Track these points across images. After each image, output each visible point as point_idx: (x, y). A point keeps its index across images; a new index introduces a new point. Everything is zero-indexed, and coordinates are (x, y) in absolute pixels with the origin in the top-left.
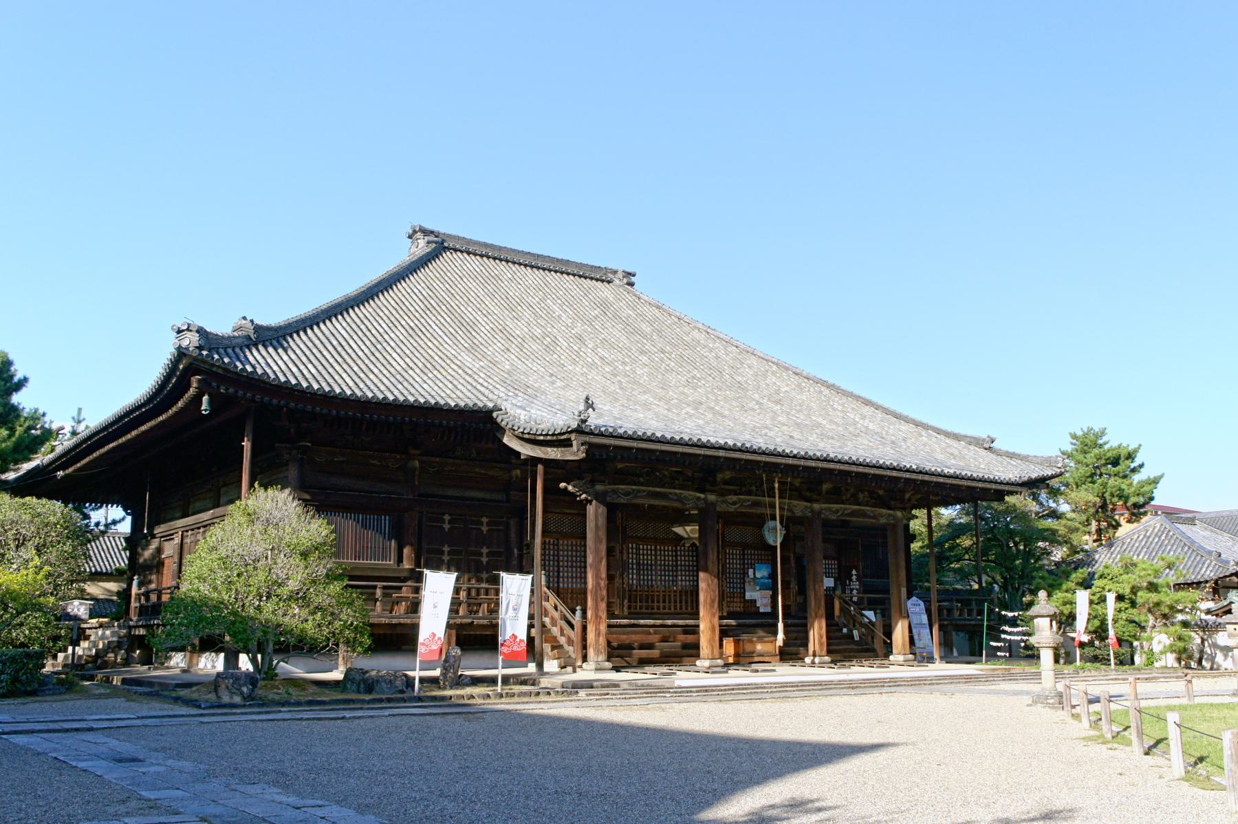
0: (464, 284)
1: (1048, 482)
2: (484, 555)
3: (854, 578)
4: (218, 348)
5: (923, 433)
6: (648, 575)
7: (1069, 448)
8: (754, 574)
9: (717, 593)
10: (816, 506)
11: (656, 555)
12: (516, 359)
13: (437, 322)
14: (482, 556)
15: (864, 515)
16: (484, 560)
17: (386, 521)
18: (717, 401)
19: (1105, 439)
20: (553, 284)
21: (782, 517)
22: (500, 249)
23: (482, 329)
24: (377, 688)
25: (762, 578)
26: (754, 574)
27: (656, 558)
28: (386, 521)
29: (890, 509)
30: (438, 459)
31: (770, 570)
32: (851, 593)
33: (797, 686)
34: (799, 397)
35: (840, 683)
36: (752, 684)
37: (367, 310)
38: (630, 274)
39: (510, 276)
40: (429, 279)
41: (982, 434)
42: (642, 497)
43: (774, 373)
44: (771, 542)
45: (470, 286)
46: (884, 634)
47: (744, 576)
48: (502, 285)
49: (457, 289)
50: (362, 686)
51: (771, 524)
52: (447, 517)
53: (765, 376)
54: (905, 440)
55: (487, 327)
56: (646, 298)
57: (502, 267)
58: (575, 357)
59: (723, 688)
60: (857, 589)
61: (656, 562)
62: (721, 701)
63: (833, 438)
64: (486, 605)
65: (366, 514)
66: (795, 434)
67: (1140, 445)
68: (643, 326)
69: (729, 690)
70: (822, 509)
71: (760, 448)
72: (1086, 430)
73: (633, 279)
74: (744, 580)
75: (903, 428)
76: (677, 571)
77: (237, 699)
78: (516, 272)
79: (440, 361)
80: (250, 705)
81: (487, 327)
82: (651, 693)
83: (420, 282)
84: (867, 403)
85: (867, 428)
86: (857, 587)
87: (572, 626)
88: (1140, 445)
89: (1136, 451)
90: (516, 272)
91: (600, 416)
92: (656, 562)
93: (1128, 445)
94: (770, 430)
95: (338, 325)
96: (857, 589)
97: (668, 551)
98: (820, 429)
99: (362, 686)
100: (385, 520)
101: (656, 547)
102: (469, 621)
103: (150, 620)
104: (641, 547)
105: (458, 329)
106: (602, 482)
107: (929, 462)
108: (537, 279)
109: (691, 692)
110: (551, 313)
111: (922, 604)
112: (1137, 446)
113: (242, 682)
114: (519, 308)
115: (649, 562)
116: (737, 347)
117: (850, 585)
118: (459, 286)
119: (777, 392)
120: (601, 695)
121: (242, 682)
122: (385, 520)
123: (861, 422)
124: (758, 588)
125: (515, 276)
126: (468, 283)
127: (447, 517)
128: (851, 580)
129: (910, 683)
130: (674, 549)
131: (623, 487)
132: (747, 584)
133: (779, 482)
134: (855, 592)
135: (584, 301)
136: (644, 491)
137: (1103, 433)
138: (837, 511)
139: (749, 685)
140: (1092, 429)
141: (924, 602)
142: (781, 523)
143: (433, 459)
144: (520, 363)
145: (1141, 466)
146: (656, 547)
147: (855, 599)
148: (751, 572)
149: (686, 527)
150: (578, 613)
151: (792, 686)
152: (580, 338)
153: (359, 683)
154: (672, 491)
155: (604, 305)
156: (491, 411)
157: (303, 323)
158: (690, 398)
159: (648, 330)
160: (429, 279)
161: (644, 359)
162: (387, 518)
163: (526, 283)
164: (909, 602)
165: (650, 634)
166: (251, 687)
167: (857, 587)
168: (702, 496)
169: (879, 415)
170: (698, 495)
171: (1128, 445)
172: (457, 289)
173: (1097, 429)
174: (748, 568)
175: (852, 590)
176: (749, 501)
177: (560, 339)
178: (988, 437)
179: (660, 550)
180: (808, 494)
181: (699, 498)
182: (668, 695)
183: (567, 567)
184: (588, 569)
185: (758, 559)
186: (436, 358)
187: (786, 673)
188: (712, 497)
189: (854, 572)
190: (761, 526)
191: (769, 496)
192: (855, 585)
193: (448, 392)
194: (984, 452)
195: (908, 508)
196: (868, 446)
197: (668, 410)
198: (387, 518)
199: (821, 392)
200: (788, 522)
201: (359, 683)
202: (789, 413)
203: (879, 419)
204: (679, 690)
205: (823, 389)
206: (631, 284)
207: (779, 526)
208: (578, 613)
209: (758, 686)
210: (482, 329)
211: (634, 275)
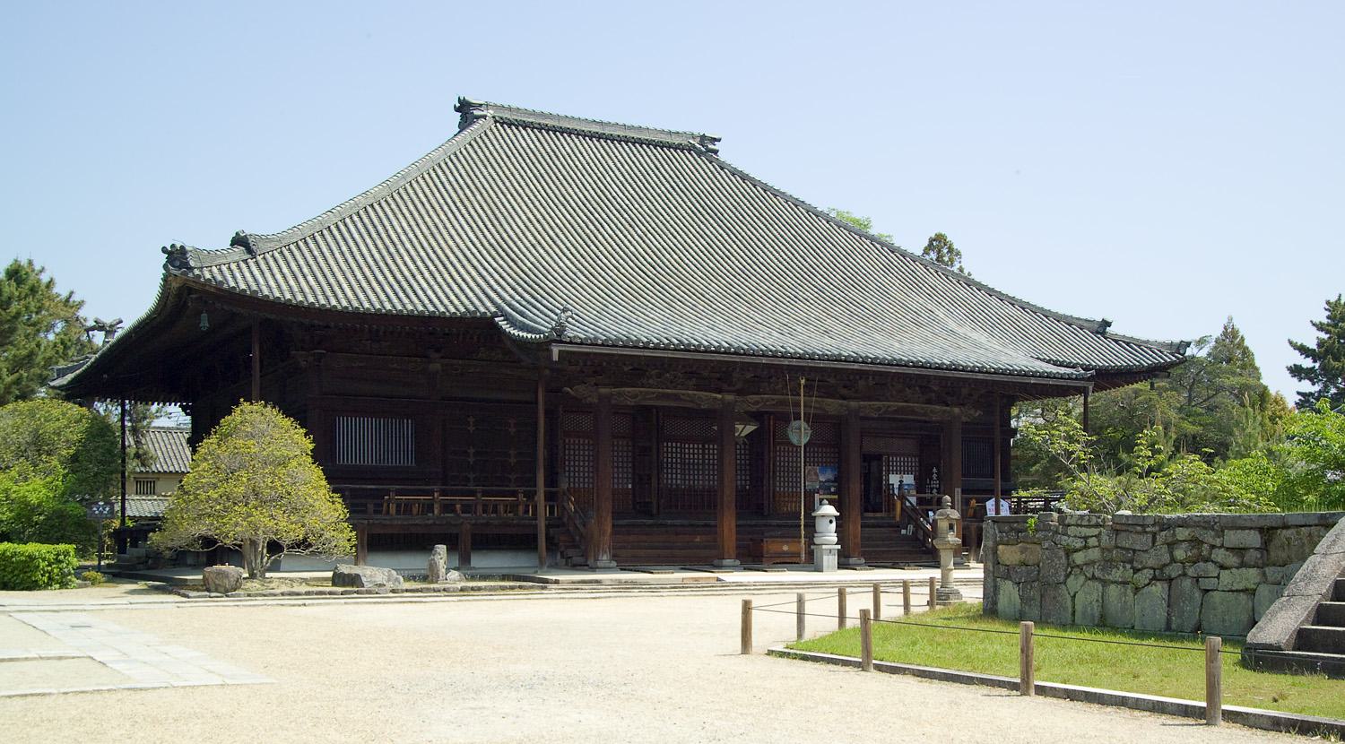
2: (471, 455)
3: (935, 476)
4: (202, 268)
6: (672, 474)
10: (853, 404)
11: (703, 454)
14: (469, 456)
15: (913, 412)
16: (471, 460)
25: (826, 481)
27: (703, 457)
28: (408, 424)
29: (948, 406)
30: (460, 362)
31: (836, 473)
42: (650, 399)
44: (795, 441)
51: (795, 424)
52: (471, 420)
61: (704, 462)
62: (305, 605)
70: (860, 407)
71: (877, 358)
73: (717, 146)
91: (1201, 342)
92: (704, 462)
101: (703, 446)
103: (536, 572)
106: (605, 385)
128: (931, 479)
131: (629, 389)
136: (653, 393)
138: (879, 409)
143: (455, 361)
146: (703, 446)
154: (684, 392)
162: (410, 421)
168: (719, 396)
170: (714, 395)
175: (932, 489)
176: (773, 400)
179: (896, 461)
180: (844, 392)
181: (716, 398)
183: (626, 473)
185: (814, 462)
188: (730, 397)
189: (935, 470)
190: (788, 421)
191: (792, 395)
198: (410, 421)
200: (815, 420)
211: (719, 140)
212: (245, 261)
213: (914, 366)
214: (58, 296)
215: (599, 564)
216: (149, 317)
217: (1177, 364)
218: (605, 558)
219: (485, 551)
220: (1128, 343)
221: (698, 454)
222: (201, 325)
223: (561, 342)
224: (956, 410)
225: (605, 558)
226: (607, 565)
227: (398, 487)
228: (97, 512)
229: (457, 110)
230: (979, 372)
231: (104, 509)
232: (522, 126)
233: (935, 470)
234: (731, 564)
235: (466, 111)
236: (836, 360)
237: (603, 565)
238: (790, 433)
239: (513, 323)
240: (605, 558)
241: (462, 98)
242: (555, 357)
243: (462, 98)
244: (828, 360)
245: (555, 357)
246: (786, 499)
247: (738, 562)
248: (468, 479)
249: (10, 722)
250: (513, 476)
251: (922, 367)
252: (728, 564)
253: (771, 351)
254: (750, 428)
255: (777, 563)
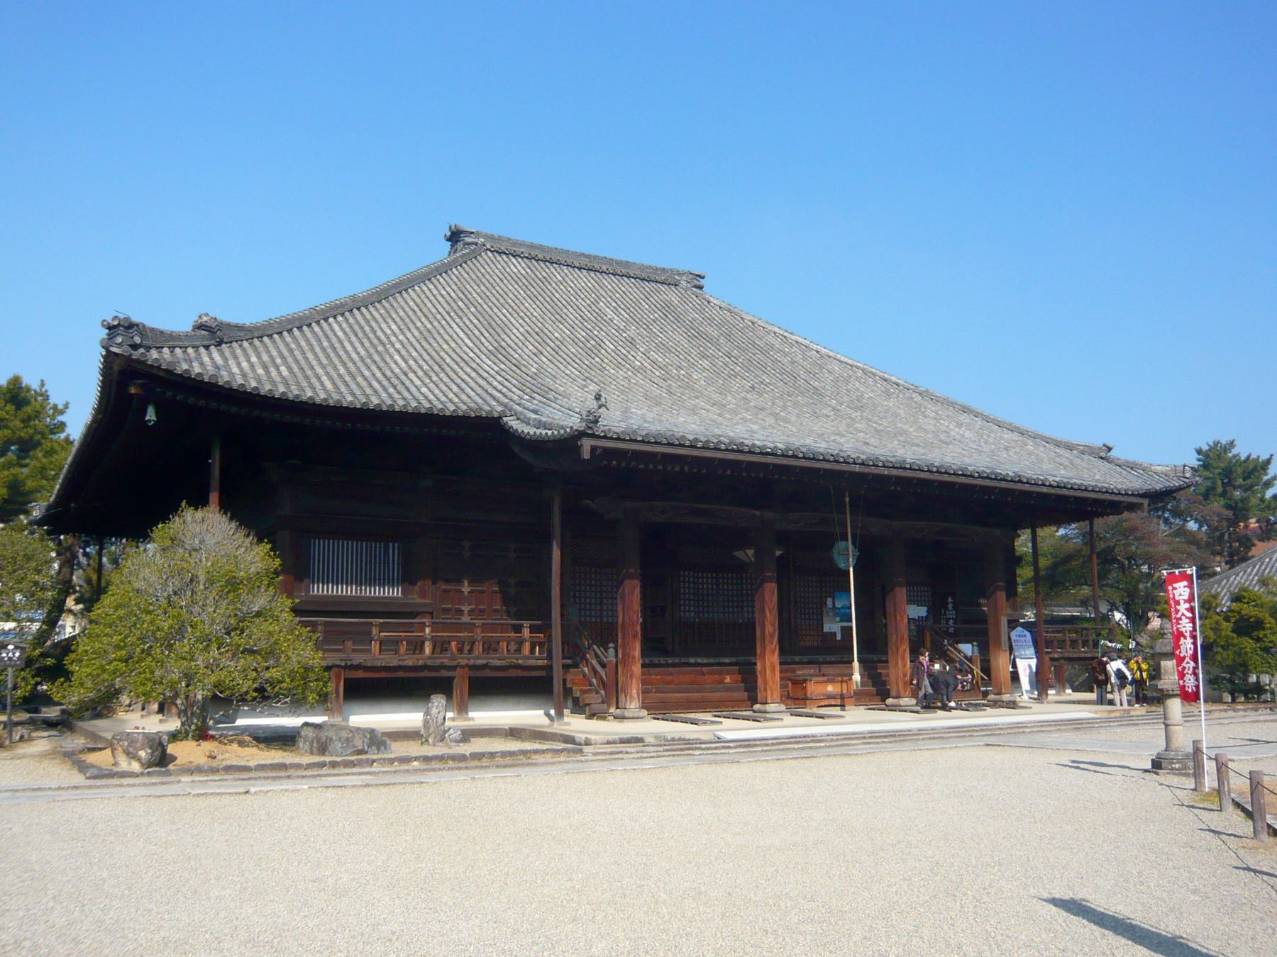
0: (503, 286)
1: (1175, 495)
3: (950, 606)
5: (1029, 442)
7: (1195, 463)
8: (834, 603)
9: (777, 626)
12: (548, 363)
13: (461, 324)
17: (394, 550)
18: (784, 408)
19: (1234, 451)
20: (609, 287)
21: (854, 536)
22: (549, 250)
23: (515, 331)
24: (331, 748)
25: (842, 608)
26: (834, 603)
28: (394, 550)
32: (947, 623)
33: (864, 738)
34: (886, 403)
35: (920, 732)
36: (856, 734)
37: (376, 312)
38: (699, 276)
39: (560, 278)
40: (463, 280)
41: (1098, 443)
43: (857, 379)
44: (842, 565)
45: (511, 287)
46: (982, 671)
47: (822, 606)
48: (549, 287)
49: (494, 292)
50: (315, 745)
51: (841, 544)
53: (847, 382)
54: (1006, 449)
55: (521, 330)
56: (716, 302)
57: (552, 269)
58: (621, 361)
59: (770, 742)
60: (953, 619)
63: (917, 445)
64: (505, 644)
65: (362, 541)
66: (872, 441)
67: (1272, 455)
68: (710, 330)
69: (777, 744)
72: (1212, 444)
74: (822, 611)
75: (1006, 436)
76: (742, 607)
77: (136, 767)
78: (569, 274)
79: (452, 364)
80: (149, 773)
81: (521, 330)
82: (677, 750)
83: (451, 283)
84: (965, 410)
85: (963, 436)
86: (954, 616)
87: (603, 666)
88: (1272, 455)
89: (1268, 462)
90: (569, 274)
93: (1258, 457)
94: (842, 436)
95: (337, 327)
96: (953, 619)
97: (707, 578)
98: (905, 436)
99: (315, 745)
100: (380, 547)
102: (484, 662)
104: (682, 573)
105: (484, 332)
107: (1030, 470)
108: (592, 281)
109: (729, 747)
110: (602, 315)
111: (1028, 634)
112: (1268, 457)
113: (138, 745)
114: (565, 310)
115: (687, 585)
116: (817, 352)
117: (945, 614)
118: (498, 288)
119: (860, 399)
120: (611, 753)
121: (138, 745)
122: (380, 547)
123: (957, 430)
124: (838, 619)
125: (566, 279)
126: (508, 285)
127: (467, 544)
129: (1006, 732)
130: (739, 575)
132: (825, 614)
133: (849, 496)
134: (951, 622)
135: (643, 303)
137: (1232, 444)
139: (804, 737)
140: (1218, 442)
141: (1030, 632)
142: (853, 543)
144: (552, 366)
145: (1274, 478)
147: (951, 630)
148: (829, 601)
149: (747, 551)
150: (612, 651)
151: (858, 738)
152: (632, 342)
153: (313, 741)
155: (667, 308)
156: (500, 418)
157: (289, 324)
158: (751, 404)
159: (715, 334)
160: (463, 280)
161: (705, 363)
162: (396, 545)
163: (578, 285)
164: (1013, 634)
165: (703, 674)
166: (149, 751)
167: (954, 616)
168: (758, 513)
169: (979, 421)
170: (753, 512)
171: (1258, 457)
172: (494, 292)
173: (1224, 442)
174: (826, 597)
175: (948, 620)
177: (607, 343)
178: (1104, 445)
182: (697, 752)
184: (757, 626)
186: (448, 360)
187: (860, 719)
189: (950, 600)
192: (951, 614)
193: (451, 395)
194: (1100, 462)
195: (1013, 529)
196: (960, 453)
197: (719, 415)
198: (396, 545)
199: (911, 398)
201: (312, 741)
202: (870, 420)
203: (978, 427)
204: (763, 742)
205: (914, 395)
206: (700, 288)
207: (851, 547)
208: (612, 651)
209: (814, 739)
210: (515, 331)
211: (703, 278)
212: (217, 367)
213: (980, 477)
214: (74, 440)
215: (627, 714)
216: (94, 421)
217: (1185, 488)
218: (633, 706)
219: (483, 697)
220: (1132, 466)
221: (712, 584)
222: (147, 418)
223: (594, 436)
224: (997, 531)
225: (633, 706)
226: (636, 715)
227: (381, 620)
228: (682, 573)
229: (448, 240)
230: (1043, 485)
231: (14, 654)
232: (512, 255)
233: (950, 600)
234: (776, 710)
235: (455, 236)
236: (901, 468)
237: (631, 715)
238: (835, 555)
239: (527, 422)
240: (633, 706)
241: (453, 227)
242: (586, 455)
243: (453, 227)
244: (893, 467)
245: (586, 455)
246: (804, 633)
247: (783, 707)
248: (460, 612)
249: (716, 397)
250: (466, 608)
251: (987, 478)
252: (772, 710)
253: (832, 456)
254: (739, 554)
255: (822, 706)
